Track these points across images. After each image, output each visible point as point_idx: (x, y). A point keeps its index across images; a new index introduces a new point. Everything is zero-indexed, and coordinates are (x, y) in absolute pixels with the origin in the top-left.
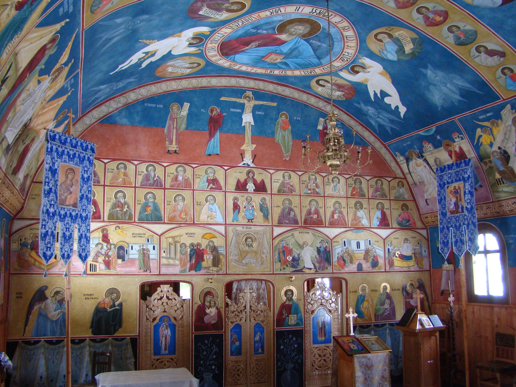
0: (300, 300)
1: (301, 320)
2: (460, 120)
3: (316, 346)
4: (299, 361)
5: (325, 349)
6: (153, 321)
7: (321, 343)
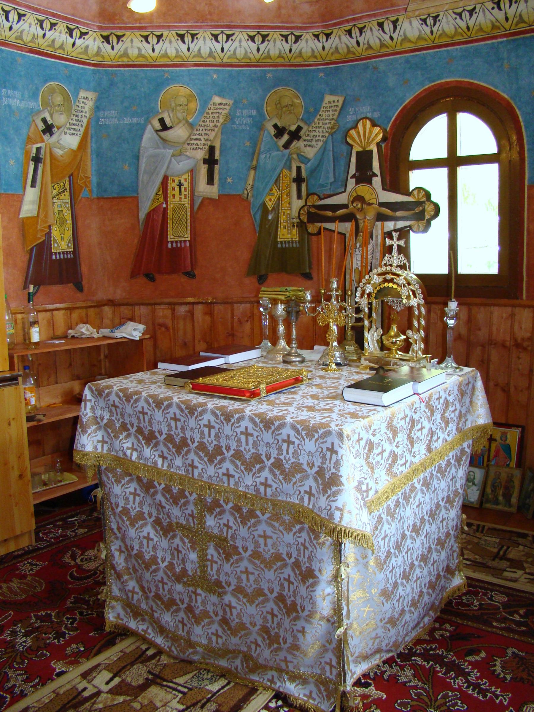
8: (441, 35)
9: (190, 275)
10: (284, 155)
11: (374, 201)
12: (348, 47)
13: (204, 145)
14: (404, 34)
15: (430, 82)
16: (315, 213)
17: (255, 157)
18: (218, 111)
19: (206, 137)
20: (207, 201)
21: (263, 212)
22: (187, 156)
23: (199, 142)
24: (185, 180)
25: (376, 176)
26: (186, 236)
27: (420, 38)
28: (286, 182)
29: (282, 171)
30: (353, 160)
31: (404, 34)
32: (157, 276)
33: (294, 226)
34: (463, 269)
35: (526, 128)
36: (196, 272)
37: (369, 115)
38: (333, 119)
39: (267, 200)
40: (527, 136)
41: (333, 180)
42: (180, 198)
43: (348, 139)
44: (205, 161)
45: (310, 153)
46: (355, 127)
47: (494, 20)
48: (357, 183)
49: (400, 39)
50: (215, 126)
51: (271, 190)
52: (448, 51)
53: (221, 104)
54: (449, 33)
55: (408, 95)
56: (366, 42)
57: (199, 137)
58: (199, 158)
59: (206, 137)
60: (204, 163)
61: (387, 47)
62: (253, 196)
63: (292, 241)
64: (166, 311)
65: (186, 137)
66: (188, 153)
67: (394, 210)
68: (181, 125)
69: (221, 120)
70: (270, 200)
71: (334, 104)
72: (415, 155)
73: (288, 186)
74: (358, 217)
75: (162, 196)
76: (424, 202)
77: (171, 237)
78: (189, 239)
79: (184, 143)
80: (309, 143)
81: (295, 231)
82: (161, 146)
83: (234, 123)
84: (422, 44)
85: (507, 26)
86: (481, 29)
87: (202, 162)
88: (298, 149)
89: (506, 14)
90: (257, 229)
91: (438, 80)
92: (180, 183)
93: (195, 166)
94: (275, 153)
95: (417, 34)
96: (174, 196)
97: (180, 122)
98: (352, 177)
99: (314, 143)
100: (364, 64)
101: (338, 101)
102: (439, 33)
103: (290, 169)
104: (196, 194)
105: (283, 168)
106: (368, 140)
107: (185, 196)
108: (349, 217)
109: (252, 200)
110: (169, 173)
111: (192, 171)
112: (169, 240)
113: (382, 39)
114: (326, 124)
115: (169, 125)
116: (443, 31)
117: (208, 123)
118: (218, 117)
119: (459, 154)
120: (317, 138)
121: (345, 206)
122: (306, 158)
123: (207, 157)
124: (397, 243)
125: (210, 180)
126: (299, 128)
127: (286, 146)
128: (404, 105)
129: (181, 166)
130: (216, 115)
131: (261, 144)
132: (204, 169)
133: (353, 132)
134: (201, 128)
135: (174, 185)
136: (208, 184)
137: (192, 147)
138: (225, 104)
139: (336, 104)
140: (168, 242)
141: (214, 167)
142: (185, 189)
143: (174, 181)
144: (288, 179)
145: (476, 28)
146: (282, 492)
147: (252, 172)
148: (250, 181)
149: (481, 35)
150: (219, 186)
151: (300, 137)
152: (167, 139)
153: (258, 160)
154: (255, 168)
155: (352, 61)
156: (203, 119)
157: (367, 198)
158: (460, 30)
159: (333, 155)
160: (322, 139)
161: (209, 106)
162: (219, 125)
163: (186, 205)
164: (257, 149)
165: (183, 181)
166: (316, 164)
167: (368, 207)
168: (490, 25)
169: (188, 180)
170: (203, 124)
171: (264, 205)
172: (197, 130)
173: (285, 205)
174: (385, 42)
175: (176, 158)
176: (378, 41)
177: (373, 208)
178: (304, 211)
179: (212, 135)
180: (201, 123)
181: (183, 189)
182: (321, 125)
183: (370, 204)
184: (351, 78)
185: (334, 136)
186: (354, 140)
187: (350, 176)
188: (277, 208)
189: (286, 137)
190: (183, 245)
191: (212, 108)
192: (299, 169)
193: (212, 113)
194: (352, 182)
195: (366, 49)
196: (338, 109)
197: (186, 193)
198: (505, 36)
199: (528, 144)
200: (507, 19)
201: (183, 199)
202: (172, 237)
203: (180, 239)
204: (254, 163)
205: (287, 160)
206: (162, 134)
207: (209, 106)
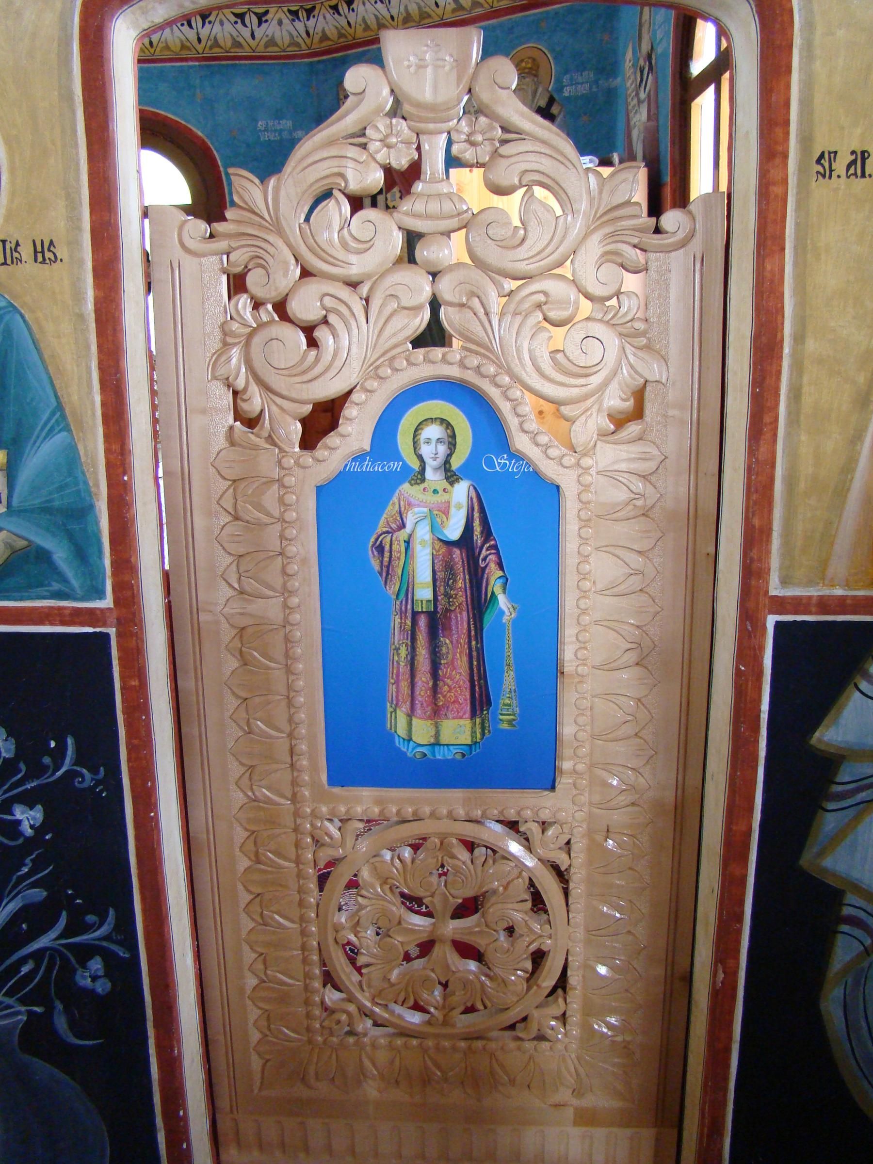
0: (44, 252)
1: (72, 517)
2: (100, 594)
3: (365, 800)
4: (92, 977)
5: (539, 957)
6: (308, 442)
7: (433, 773)
47: (184, 38)
85: (200, 48)
86: (167, 47)
145: (160, 45)
149: (167, 55)
168: (179, 45)
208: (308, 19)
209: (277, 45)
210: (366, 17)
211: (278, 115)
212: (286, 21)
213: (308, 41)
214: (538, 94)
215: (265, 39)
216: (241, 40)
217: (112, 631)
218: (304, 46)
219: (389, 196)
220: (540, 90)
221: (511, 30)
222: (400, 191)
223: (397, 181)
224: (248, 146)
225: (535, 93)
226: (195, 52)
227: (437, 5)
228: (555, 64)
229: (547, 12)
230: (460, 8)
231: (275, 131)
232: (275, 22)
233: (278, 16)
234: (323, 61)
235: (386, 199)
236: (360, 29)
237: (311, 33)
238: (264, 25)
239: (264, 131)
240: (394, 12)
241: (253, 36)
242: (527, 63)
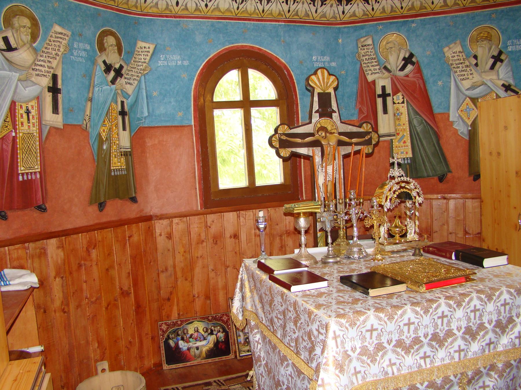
8: (243, 11)
9: (42, 209)
10: (111, 90)
11: (336, 131)
12: (167, 4)
13: (48, 72)
14: (218, 5)
15: (230, 44)
16: (286, 140)
17: (91, 89)
18: (59, 40)
19: (49, 65)
20: (54, 130)
21: (99, 143)
22: (33, 82)
23: (43, 69)
24: (33, 107)
25: (336, 112)
26: (36, 167)
27: (228, 10)
28: (115, 115)
29: (111, 104)
30: (316, 98)
31: (218, 5)
32: (9, 213)
33: (122, 155)
34: (259, 182)
35: (297, 84)
36: (47, 206)
37: (327, 65)
38: (145, 62)
39: (102, 131)
40: (299, 90)
41: (147, 114)
42: (29, 126)
43: (310, 83)
44: (50, 89)
45: (130, 89)
46: (315, 73)
47: (281, 9)
48: (320, 117)
49: (213, 7)
50: (57, 54)
51: (104, 122)
52: (245, 23)
53: (61, 33)
54: (249, 12)
55: (212, 51)
56: (184, 4)
57: (43, 63)
58: (44, 86)
59: (49, 65)
60: (49, 91)
61: (201, 12)
62: (90, 126)
63: (122, 169)
64: (20, 251)
65: (31, 61)
66: (33, 79)
67: (351, 138)
68: (25, 48)
69: (62, 50)
70: (104, 131)
71: (145, 50)
72: (217, 98)
73: (116, 118)
74: (323, 143)
75: (10, 123)
76: (371, 132)
77: (21, 169)
78: (39, 170)
79: (29, 68)
80: (129, 81)
81: (123, 160)
82: (6, 67)
83: (72, 54)
84: (228, 15)
85: (288, 15)
86: (271, 14)
87: (47, 90)
88: (122, 85)
89: (289, 7)
90: (96, 158)
91: (236, 43)
92: (28, 110)
93: (41, 93)
94: (105, 87)
95: (227, 6)
96: (22, 124)
97: (25, 44)
98: (316, 112)
99: (131, 81)
100: (177, 21)
101: (149, 48)
102: (243, 10)
103: (116, 102)
104: (43, 123)
105: (112, 101)
106: (327, 85)
107: (34, 125)
108: (316, 144)
109: (90, 130)
110: (16, 99)
111: (38, 98)
112: (20, 172)
113: (199, 5)
114: (139, 66)
115: (14, 45)
116: (246, 9)
117: (50, 51)
118: (59, 46)
119: (252, 98)
120: (134, 77)
121: (312, 135)
122: (127, 94)
123: (51, 85)
124: (396, 162)
125: (55, 110)
126: (121, 67)
127: (113, 82)
128: (209, 58)
129: (28, 92)
130: (57, 44)
131: (95, 77)
132: (49, 97)
133: (313, 77)
134: (44, 55)
135: (22, 111)
136: (53, 113)
137: (37, 73)
138: (65, 35)
139: (147, 50)
140: (18, 174)
141: (57, 96)
142: (33, 117)
143: (21, 107)
144: (115, 112)
145: (268, 12)
146: (370, 374)
147: (89, 103)
148: (88, 113)
149: (270, 17)
150: (63, 115)
151: (122, 75)
152: (13, 61)
153: (93, 93)
154: (91, 100)
155: (167, 17)
156: (46, 46)
157: (329, 128)
158: (257, 11)
159: (146, 93)
160: (137, 78)
161: (51, 34)
162: (60, 53)
163: (35, 134)
164: (92, 82)
165: (30, 108)
166: (134, 100)
167: (331, 135)
168: (278, 12)
169: (36, 108)
170: (46, 50)
171: (99, 135)
172: (41, 56)
173: (114, 136)
174: (200, 8)
175: (22, 83)
176: (194, 5)
177: (335, 136)
178: (276, 138)
179: (54, 63)
180: (44, 50)
181: (31, 117)
182: (135, 66)
183: (331, 133)
184: (162, 30)
185: (147, 77)
186: (316, 84)
187: (314, 111)
188: (109, 139)
189: (112, 74)
190: (34, 177)
191: (54, 35)
192: (122, 103)
193: (54, 41)
194: (316, 117)
195: (183, 10)
196: (150, 54)
197: (34, 121)
198: (284, 21)
199: (299, 95)
200: (289, 11)
201: (32, 128)
202: (23, 168)
203: (31, 171)
204: (90, 95)
205: (114, 94)
206: (8, 54)
207: (51, 34)
208: (347, 5)
209: (326, 17)
210: (386, 7)
211: (323, 54)
212: (335, 5)
213: (342, 16)
214: (492, 49)
215: (322, 13)
216: (310, 13)
217: (166, 367)
218: (338, 19)
219: (395, 97)
220: (493, 47)
221: (473, 18)
222: (403, 95)
223: (400, 89)
224: (308, 69)
225: (490, 49)
226: (284, 16)
227: (433, 3)
228: (502, 35)
229: (497, 10)
230: (446, 5)
231: (322, 62)
232: (329, 5)
233: (331, 2)
234: (348, 27)
235: (393, 99)
236: (378, 12)
237: (346, 12)
238: (324, 6)
239: (316, 61)
240: (404, 5)
241: (373, 9)
242: (484, 34)
